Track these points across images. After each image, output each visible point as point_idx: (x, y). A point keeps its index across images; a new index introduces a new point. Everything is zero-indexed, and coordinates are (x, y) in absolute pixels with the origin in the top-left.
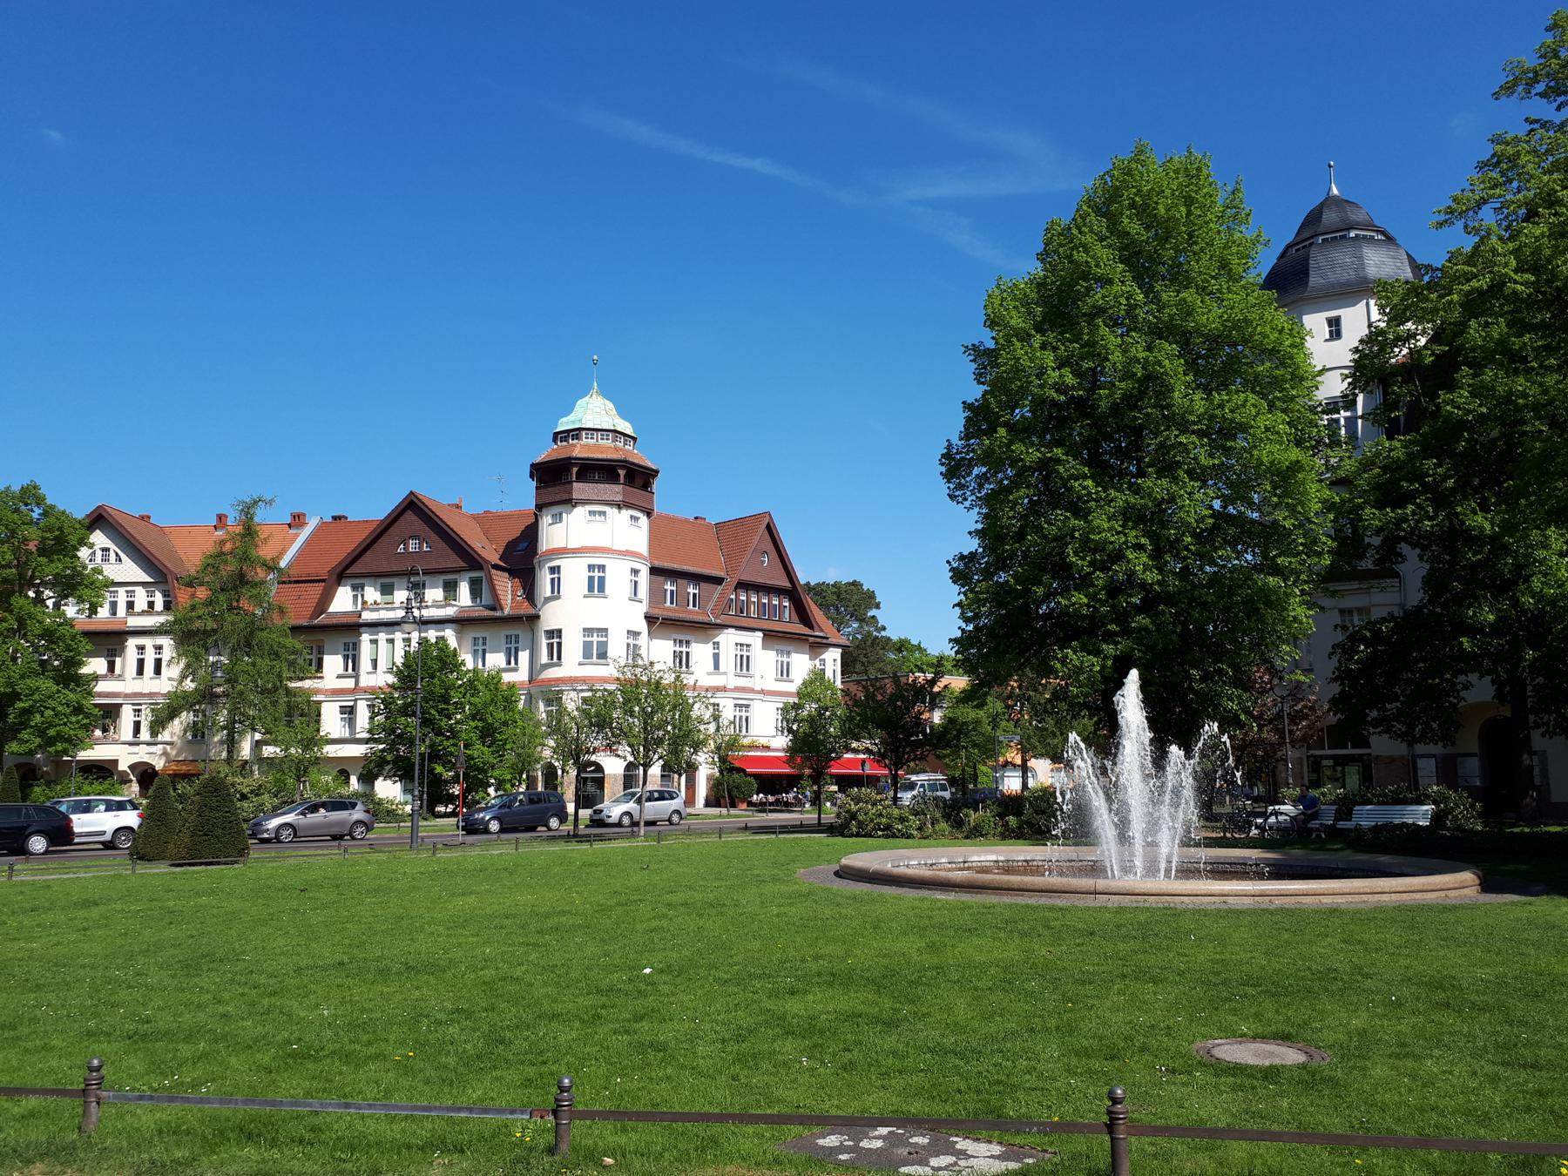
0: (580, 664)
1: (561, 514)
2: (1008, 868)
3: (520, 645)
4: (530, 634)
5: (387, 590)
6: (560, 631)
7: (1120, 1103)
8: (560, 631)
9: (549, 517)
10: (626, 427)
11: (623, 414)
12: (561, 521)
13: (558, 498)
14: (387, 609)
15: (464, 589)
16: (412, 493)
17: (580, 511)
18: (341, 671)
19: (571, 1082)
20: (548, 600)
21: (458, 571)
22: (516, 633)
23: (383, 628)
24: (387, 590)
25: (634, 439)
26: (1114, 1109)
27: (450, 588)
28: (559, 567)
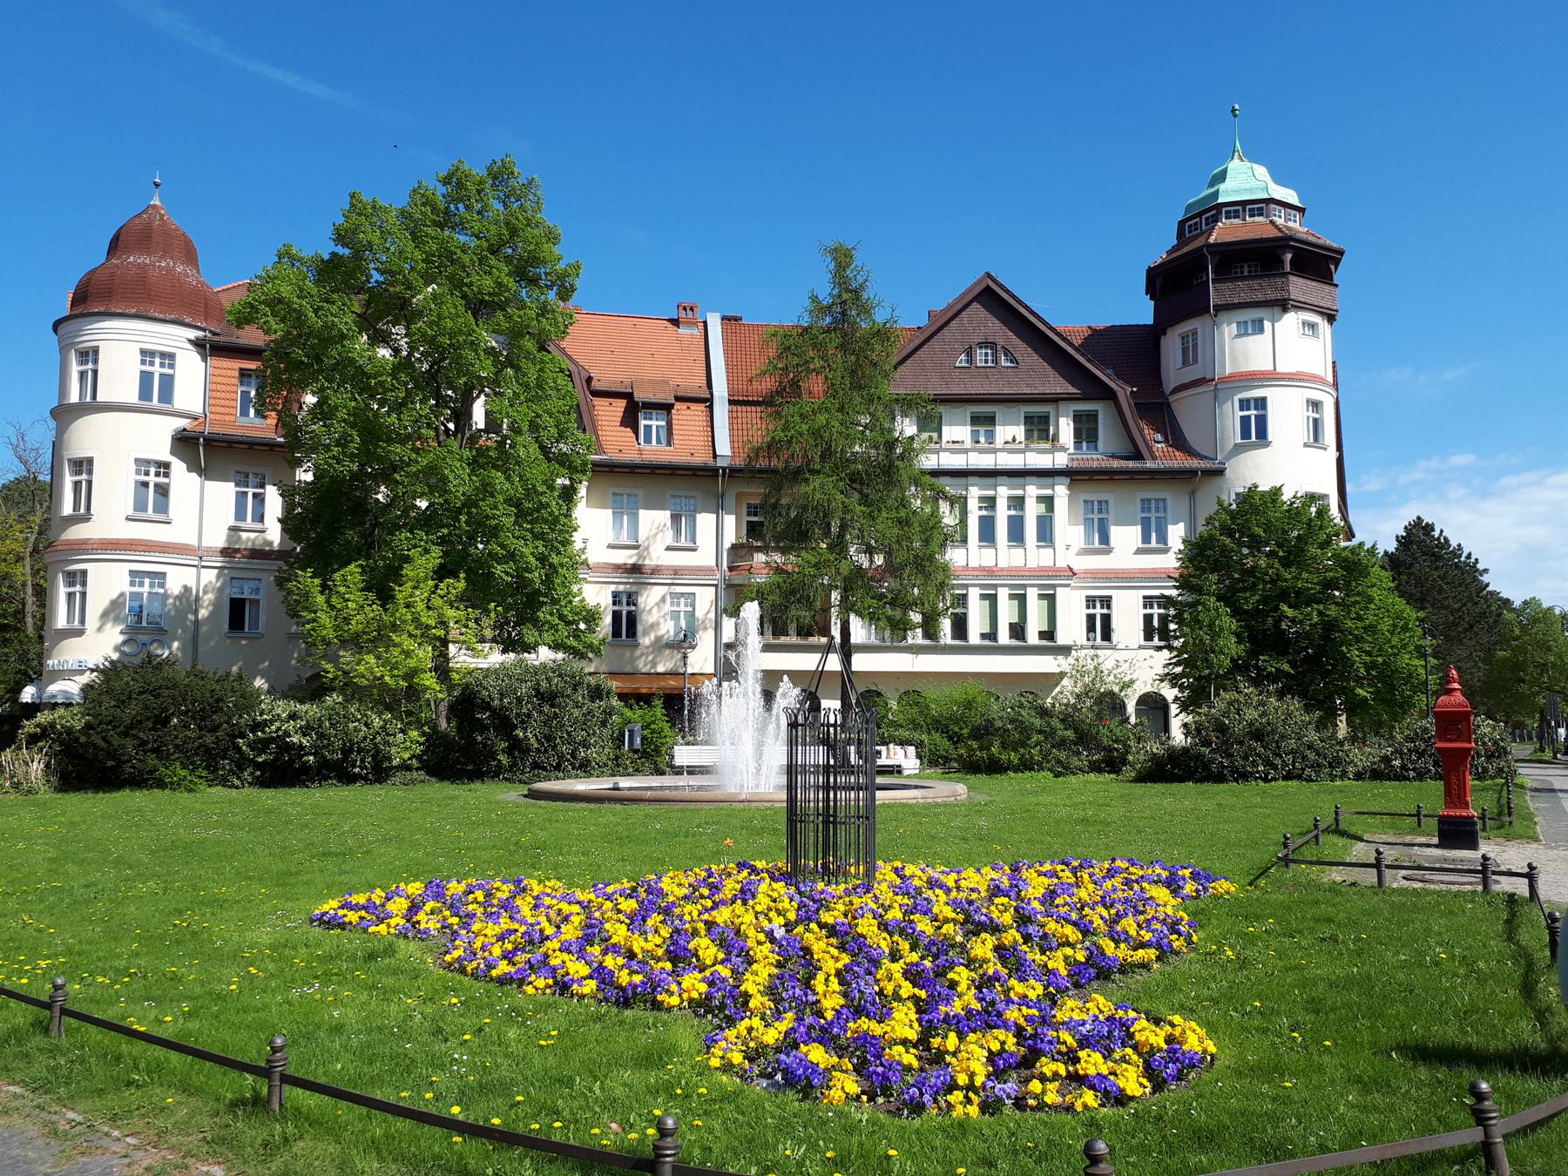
0: (128, 519)
1: (1261, 321)
2: (1438, 860)
3: (1111, 517)
4: (1185, 501)
5: (985, 422)
6: (90, 461)
7: (672, 1135)
8: (90, 461)
9: (1234, 326)
10: (1291, 196)
11: (1279, 180)
12: (1261, 331)
13: (1260, 297)
14: (953, 451)
15: (1066, 429)
16: (988, 275)
17: (1291, 321)
18: (130, 511)
19: (675, 1123)
20: (1238, 449)
21: (1055, 400)
22: (1102, 497)
23: (1034, 479)
24: (985, 422)
25: (1301, 210)
26: (661, 1144)
27: (1039, 429)
28: (1264, 400)
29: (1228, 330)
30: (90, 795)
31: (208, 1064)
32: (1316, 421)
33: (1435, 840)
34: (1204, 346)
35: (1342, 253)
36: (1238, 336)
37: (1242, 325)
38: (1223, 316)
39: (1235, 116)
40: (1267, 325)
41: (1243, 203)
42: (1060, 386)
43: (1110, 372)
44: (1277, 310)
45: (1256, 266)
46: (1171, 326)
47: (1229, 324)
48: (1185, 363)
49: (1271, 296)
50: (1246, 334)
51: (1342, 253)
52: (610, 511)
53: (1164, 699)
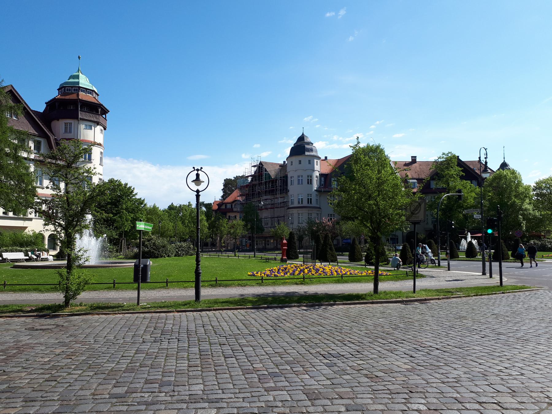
1: (91, 126)
12: (91, 129)
13: (92, 119)
29: (82, 126)
30: (319, 293)
31: (499, 276)
32: (101, 157)
33: (482, 274)
34: (74, 129)
35: (109, 112)
36: (85, 129)
37: (86, 125)
38: (81, 122)
39: (79, 59)
40: (93, 128)
41: (87, 89)
42: (32, 131)
43: (48, 130)
44: (96, 124)
45: (88, 109)
46: (62, 119)
47: (83, 125)
48: (66, 131)
49: (95, 120)
50: (87, 129)
51: (109, 112)
52: (148, 206)
53: (365, 261)
